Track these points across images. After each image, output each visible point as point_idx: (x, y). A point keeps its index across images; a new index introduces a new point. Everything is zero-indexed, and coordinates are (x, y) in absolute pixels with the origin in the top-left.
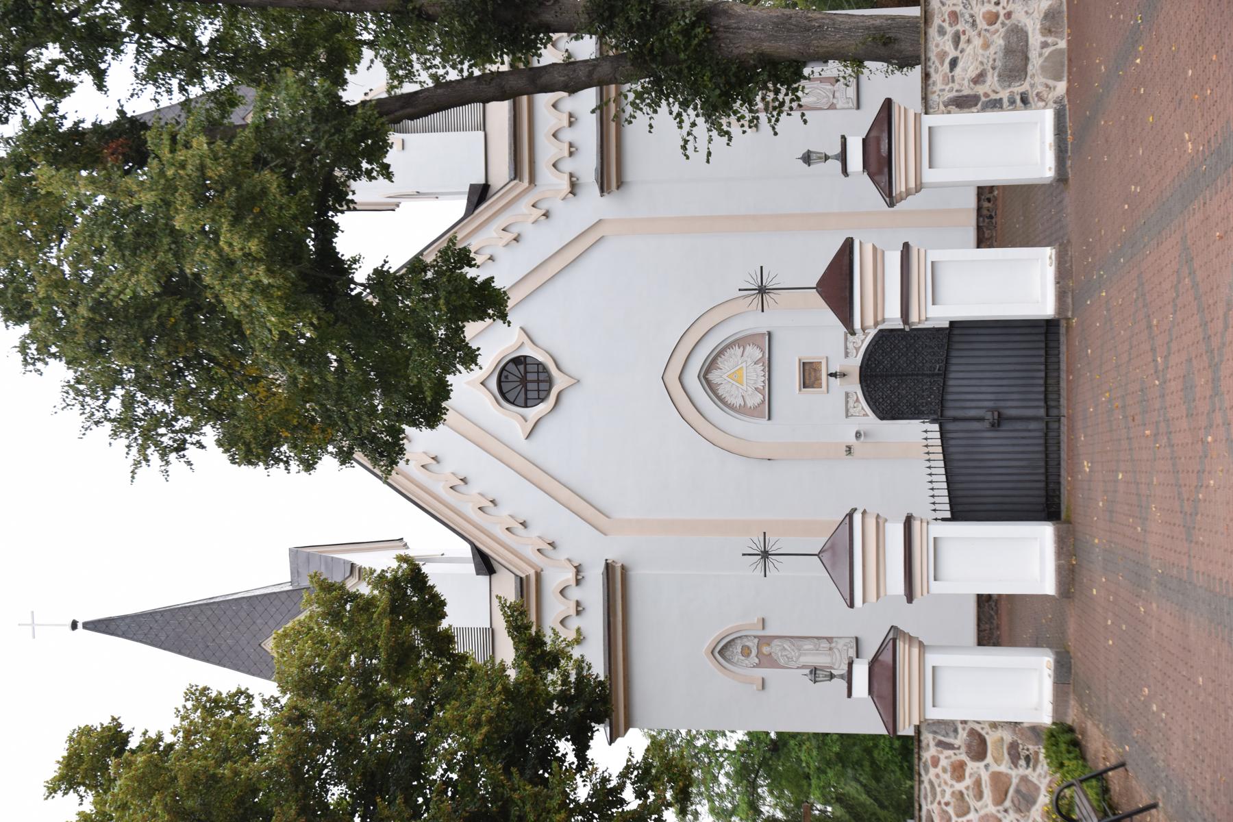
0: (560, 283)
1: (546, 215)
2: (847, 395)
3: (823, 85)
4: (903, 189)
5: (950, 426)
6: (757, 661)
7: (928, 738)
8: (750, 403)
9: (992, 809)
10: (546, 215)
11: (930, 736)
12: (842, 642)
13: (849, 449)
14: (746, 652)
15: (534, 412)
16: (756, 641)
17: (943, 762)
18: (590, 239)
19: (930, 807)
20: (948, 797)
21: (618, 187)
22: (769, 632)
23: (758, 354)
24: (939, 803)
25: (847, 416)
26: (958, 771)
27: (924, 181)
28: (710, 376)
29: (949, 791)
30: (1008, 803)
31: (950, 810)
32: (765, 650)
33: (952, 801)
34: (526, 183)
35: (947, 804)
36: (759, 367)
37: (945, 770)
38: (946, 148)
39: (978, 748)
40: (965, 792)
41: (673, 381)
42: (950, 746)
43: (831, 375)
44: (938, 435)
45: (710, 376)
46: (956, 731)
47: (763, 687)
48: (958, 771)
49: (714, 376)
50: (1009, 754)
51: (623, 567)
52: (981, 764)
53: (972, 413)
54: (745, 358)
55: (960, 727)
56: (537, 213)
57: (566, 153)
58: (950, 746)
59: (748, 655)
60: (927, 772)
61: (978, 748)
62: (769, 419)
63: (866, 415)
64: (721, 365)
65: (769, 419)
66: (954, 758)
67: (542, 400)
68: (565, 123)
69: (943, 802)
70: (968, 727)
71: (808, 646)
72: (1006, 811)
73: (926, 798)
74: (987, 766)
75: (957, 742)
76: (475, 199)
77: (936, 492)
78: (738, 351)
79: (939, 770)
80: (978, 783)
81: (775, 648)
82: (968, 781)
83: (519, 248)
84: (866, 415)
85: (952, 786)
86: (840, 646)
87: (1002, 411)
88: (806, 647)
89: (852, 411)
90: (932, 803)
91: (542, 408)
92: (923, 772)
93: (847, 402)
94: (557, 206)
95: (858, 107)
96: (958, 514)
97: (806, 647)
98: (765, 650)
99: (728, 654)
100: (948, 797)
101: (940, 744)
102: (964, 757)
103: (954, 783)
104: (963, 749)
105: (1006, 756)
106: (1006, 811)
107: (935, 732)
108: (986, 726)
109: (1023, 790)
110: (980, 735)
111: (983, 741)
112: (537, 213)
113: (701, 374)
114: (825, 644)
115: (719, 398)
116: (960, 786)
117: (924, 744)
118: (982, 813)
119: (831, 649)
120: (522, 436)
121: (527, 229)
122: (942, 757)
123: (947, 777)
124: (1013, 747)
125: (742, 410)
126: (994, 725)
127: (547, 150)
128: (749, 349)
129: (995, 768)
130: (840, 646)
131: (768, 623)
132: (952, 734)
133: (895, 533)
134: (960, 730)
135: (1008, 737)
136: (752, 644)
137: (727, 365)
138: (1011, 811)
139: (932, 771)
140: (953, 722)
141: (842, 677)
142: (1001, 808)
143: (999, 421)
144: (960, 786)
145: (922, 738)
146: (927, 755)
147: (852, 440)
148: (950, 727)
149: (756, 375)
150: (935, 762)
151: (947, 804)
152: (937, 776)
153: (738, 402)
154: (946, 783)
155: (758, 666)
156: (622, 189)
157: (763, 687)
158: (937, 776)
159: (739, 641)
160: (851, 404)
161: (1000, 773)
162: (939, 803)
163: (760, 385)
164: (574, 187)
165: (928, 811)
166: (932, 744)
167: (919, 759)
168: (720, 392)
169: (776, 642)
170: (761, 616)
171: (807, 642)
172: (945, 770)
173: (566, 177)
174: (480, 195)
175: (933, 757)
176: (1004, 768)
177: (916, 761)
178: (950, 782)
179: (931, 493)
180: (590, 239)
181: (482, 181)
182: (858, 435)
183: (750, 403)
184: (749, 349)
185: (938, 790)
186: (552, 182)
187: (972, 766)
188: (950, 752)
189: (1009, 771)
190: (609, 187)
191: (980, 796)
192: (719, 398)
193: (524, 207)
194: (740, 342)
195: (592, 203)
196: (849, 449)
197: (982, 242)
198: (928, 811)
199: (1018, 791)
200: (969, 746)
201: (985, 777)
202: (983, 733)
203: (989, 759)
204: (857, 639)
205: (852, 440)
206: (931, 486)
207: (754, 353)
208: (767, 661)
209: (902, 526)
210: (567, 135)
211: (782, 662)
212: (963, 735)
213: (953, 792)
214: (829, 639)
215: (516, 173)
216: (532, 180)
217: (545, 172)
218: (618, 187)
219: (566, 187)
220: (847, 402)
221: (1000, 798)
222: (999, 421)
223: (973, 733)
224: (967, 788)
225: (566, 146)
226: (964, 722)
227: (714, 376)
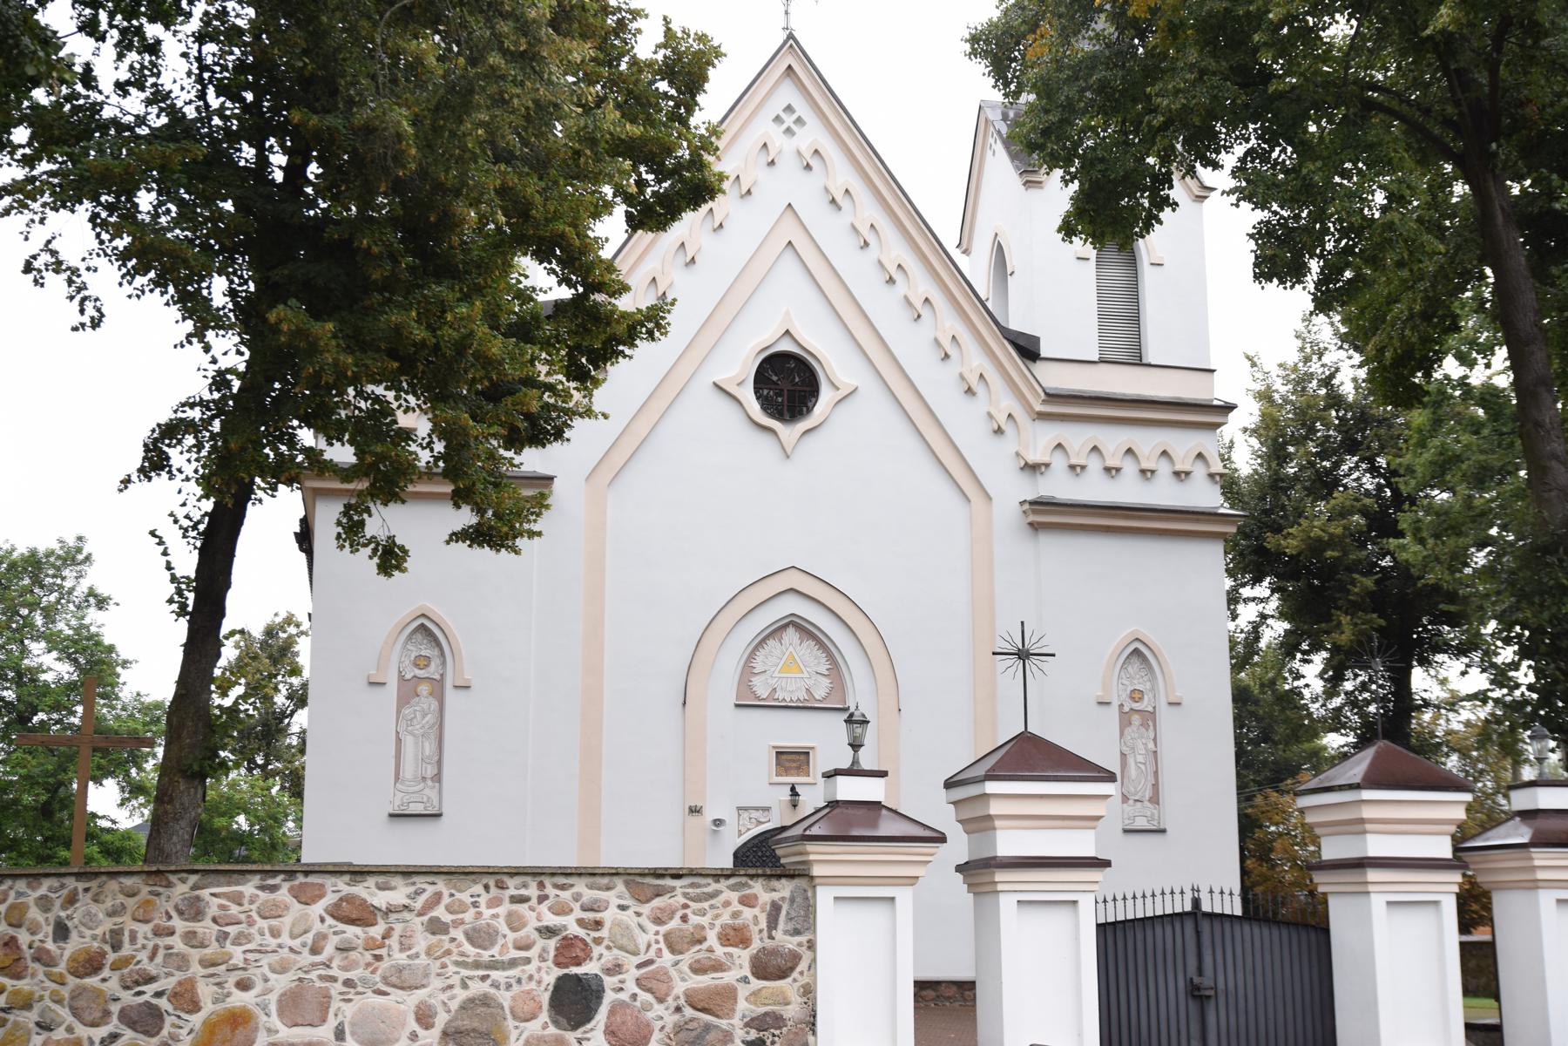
0: (913, 443)
1: (999, 431)
2: (767, 809)
3: (1149, 786)
4: (1537, 863)
5: (1189, 926)
6: (408, 676)
7: (785, 889)
8: (756, 681)
9: (680, 988)
10: (999, 431)
11: (786, 893)
12: (433, 794)
13: (695, 811)
14: (421, 662)
15: (748, 395)
16: (437, 677)
17: (748, 913)
18: (968, 485)
19: (679, 891)
20: (694, 919)
21: (1031, 524)
22: (451, 696)
23: (820, 693)
24: (685, 906)
25: (739, 809)
26: (735, 936)
27: (1541, 892)
28: (791, 630)
29: (704, 921)
30: (689, 1012)
31: (675, 923)
32: (424, 689)
33: (689, 927)
34: (1039, 408)
35: (684, 919)
36: (802, 695)
37: (735, 915)
38: (1416, 925)
39: (771, 967)
40: (705, 946)
41: (794, 581)
42: (773, 923)
43: (794, 792)
44: (1178, 910)
45: (791, 630)
46: (797, 932)
47: (372, 684)
48: (735, 936)
49: (791, 635)
50: (766, 1014)
51: (1219, 425)
52: (747, 972)
53: (1208, 959)
54: (815, 676)
55: (803, 939)
56: (1002, 419)
57: (1074, 461)
58: (773, 923)
59: (417, 665)
60: (732, 888)
61: (771, 967)
62: (737, 706)
63: (740, 834)
64: (805, 644)
65: (737, 706)
66: (754, 930)
67: (765, 408)
68: (1110, 463)
69: (688, 911)
70: (803, 951)
71: (429, 748)
72: (678, 1009)
73: (692, 885)
74: (745, 980)
75: (778, 934)
76: (1021, 342)
77: (1159, 899)
78: (823, 669)
79: (736, 906)
80: (718, 967)
81: (427, 703)
82: (720, 951)
83: (957, 392)
84: (740, 834)
85: (712, 925)
86: (427, 791)
87: (1213, 1001)
88: (427, 745)
89: (745, 815)
90: (685, 895)
91: (754, 407)
92: (732, 881)
93: (757, 809)
94: (1009, 444)
95: (1126, 831)
96: (1106, 931)
97: (427, 745)
98: (424, 689)
99: (419, 636)
100: (694, 919)
101: (775, 908)
102: (756, 945)
103: (717, 929)
104: (768, 943)
105: (763, 1009)
106: (678, 1009)
107: (792, 900)
108: (805, 980)
109: (710, 1037)
110: (792, 969)
111: (782, 974)
112: (1002, 419)
113: (800, 618)
114: (430, 771)
115: (764, 640)
116: (712, 939)
117: (775, 883)
118: (673, 973)
119: (424, 779)
120: (718, 379)
121: (981, 405)
122: (756, 911)
123: (726, 918)
124: (777, 1020)
125: (748, 670)
126: (808, 992)
127: (1078, 437)
128: (826, 682)
129: (743, 992)
130: (427, 791)
131: (462, 693)
132: (790, 926)
133: (1080, 844)
134: (798, 939)
135: (793, 1011)
136: (433, 671)
137: (806, 653)
138: (677, 1017)
139: (734, 896)
140: (812, 928)
141: (855, 761)
142: (682, 1001)
143: (1196, 994)
144: (712, 939)
145: (783, 881)
146: (757, 887)
147: (710, 814)
148: (805, 920)
149: (792, 691)
150: (747, 901)
151: (684, 919)
152: (727, 904)
153: (759, 665)
154: (717, 916)
155: (401, 678)
156: (1029, 530)
157: (372, 684)
158: (727, 904)
159: (436, 652)
160: (755, 814)
161: (735, 1000)
162: (685, 906)
163: (780, 695)
164: (1033, 468)
165: (674, 889)
166: (776, 896)
167: (752, 877)
168: (771, 642)
169: (435, 704)
170: (472, 684)
171: (435, 745)
172: (735, 915)
173: (1046, 459)
174: (1027, 349)
175: (756, 897)
176: (743, 1006)
177: (752, 871)
178: (718, 923)
179: (1120, 897)
180: (968, 485)
181: (1043, 354)
182: (718, 822)
183: (756, 681)
184: (826, 682)
185: (706, 905)
186: (1040, 441)
187: (743, 956)
188: (763, 924)
189: (738, 1015)
190: (1035, 512)
191: (698, 969)
192: (764, 640)
193: (1006, 403)
194: (836, 670)
195: (1011, 492)
196: (695, 811)
197: (920, 986)
198: (674, 889)
199: (708, 1028)
200: (774, 952)
201: (729, 977)
202: (795, 974)
203: (756, 984)
204: (439, 815)
205: (710, 814)
206: (1148, 894)
207: (821, 688)
208: (408, 691)
209: (1092, 854)
210: (1094, 465)
211: (406, 711)
212: (791, 943)
213: (703, 928)
214: (438, 778)
215: (1052, 397)
216: (1042, 416)
217: (1050, 433)
218: (1031, 524)
219: (1033, 458)
220: (757, 809)
221: (699, 1002)
222: (1196, 994)
223: (795, 958)
224: (710, 950)
225: (1082, 462)
226: (811, 946)
227: (791, 635)
